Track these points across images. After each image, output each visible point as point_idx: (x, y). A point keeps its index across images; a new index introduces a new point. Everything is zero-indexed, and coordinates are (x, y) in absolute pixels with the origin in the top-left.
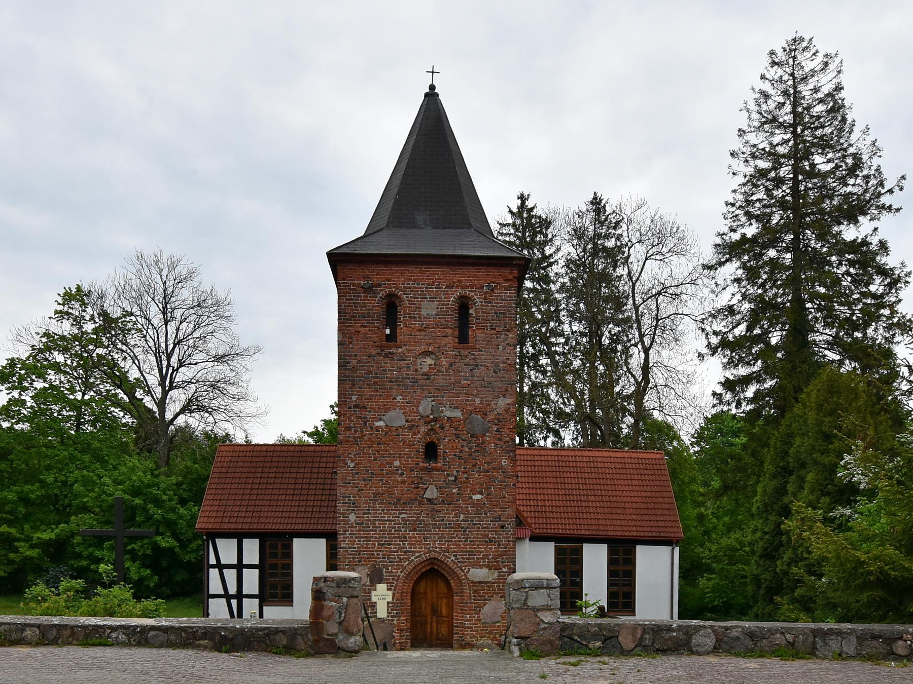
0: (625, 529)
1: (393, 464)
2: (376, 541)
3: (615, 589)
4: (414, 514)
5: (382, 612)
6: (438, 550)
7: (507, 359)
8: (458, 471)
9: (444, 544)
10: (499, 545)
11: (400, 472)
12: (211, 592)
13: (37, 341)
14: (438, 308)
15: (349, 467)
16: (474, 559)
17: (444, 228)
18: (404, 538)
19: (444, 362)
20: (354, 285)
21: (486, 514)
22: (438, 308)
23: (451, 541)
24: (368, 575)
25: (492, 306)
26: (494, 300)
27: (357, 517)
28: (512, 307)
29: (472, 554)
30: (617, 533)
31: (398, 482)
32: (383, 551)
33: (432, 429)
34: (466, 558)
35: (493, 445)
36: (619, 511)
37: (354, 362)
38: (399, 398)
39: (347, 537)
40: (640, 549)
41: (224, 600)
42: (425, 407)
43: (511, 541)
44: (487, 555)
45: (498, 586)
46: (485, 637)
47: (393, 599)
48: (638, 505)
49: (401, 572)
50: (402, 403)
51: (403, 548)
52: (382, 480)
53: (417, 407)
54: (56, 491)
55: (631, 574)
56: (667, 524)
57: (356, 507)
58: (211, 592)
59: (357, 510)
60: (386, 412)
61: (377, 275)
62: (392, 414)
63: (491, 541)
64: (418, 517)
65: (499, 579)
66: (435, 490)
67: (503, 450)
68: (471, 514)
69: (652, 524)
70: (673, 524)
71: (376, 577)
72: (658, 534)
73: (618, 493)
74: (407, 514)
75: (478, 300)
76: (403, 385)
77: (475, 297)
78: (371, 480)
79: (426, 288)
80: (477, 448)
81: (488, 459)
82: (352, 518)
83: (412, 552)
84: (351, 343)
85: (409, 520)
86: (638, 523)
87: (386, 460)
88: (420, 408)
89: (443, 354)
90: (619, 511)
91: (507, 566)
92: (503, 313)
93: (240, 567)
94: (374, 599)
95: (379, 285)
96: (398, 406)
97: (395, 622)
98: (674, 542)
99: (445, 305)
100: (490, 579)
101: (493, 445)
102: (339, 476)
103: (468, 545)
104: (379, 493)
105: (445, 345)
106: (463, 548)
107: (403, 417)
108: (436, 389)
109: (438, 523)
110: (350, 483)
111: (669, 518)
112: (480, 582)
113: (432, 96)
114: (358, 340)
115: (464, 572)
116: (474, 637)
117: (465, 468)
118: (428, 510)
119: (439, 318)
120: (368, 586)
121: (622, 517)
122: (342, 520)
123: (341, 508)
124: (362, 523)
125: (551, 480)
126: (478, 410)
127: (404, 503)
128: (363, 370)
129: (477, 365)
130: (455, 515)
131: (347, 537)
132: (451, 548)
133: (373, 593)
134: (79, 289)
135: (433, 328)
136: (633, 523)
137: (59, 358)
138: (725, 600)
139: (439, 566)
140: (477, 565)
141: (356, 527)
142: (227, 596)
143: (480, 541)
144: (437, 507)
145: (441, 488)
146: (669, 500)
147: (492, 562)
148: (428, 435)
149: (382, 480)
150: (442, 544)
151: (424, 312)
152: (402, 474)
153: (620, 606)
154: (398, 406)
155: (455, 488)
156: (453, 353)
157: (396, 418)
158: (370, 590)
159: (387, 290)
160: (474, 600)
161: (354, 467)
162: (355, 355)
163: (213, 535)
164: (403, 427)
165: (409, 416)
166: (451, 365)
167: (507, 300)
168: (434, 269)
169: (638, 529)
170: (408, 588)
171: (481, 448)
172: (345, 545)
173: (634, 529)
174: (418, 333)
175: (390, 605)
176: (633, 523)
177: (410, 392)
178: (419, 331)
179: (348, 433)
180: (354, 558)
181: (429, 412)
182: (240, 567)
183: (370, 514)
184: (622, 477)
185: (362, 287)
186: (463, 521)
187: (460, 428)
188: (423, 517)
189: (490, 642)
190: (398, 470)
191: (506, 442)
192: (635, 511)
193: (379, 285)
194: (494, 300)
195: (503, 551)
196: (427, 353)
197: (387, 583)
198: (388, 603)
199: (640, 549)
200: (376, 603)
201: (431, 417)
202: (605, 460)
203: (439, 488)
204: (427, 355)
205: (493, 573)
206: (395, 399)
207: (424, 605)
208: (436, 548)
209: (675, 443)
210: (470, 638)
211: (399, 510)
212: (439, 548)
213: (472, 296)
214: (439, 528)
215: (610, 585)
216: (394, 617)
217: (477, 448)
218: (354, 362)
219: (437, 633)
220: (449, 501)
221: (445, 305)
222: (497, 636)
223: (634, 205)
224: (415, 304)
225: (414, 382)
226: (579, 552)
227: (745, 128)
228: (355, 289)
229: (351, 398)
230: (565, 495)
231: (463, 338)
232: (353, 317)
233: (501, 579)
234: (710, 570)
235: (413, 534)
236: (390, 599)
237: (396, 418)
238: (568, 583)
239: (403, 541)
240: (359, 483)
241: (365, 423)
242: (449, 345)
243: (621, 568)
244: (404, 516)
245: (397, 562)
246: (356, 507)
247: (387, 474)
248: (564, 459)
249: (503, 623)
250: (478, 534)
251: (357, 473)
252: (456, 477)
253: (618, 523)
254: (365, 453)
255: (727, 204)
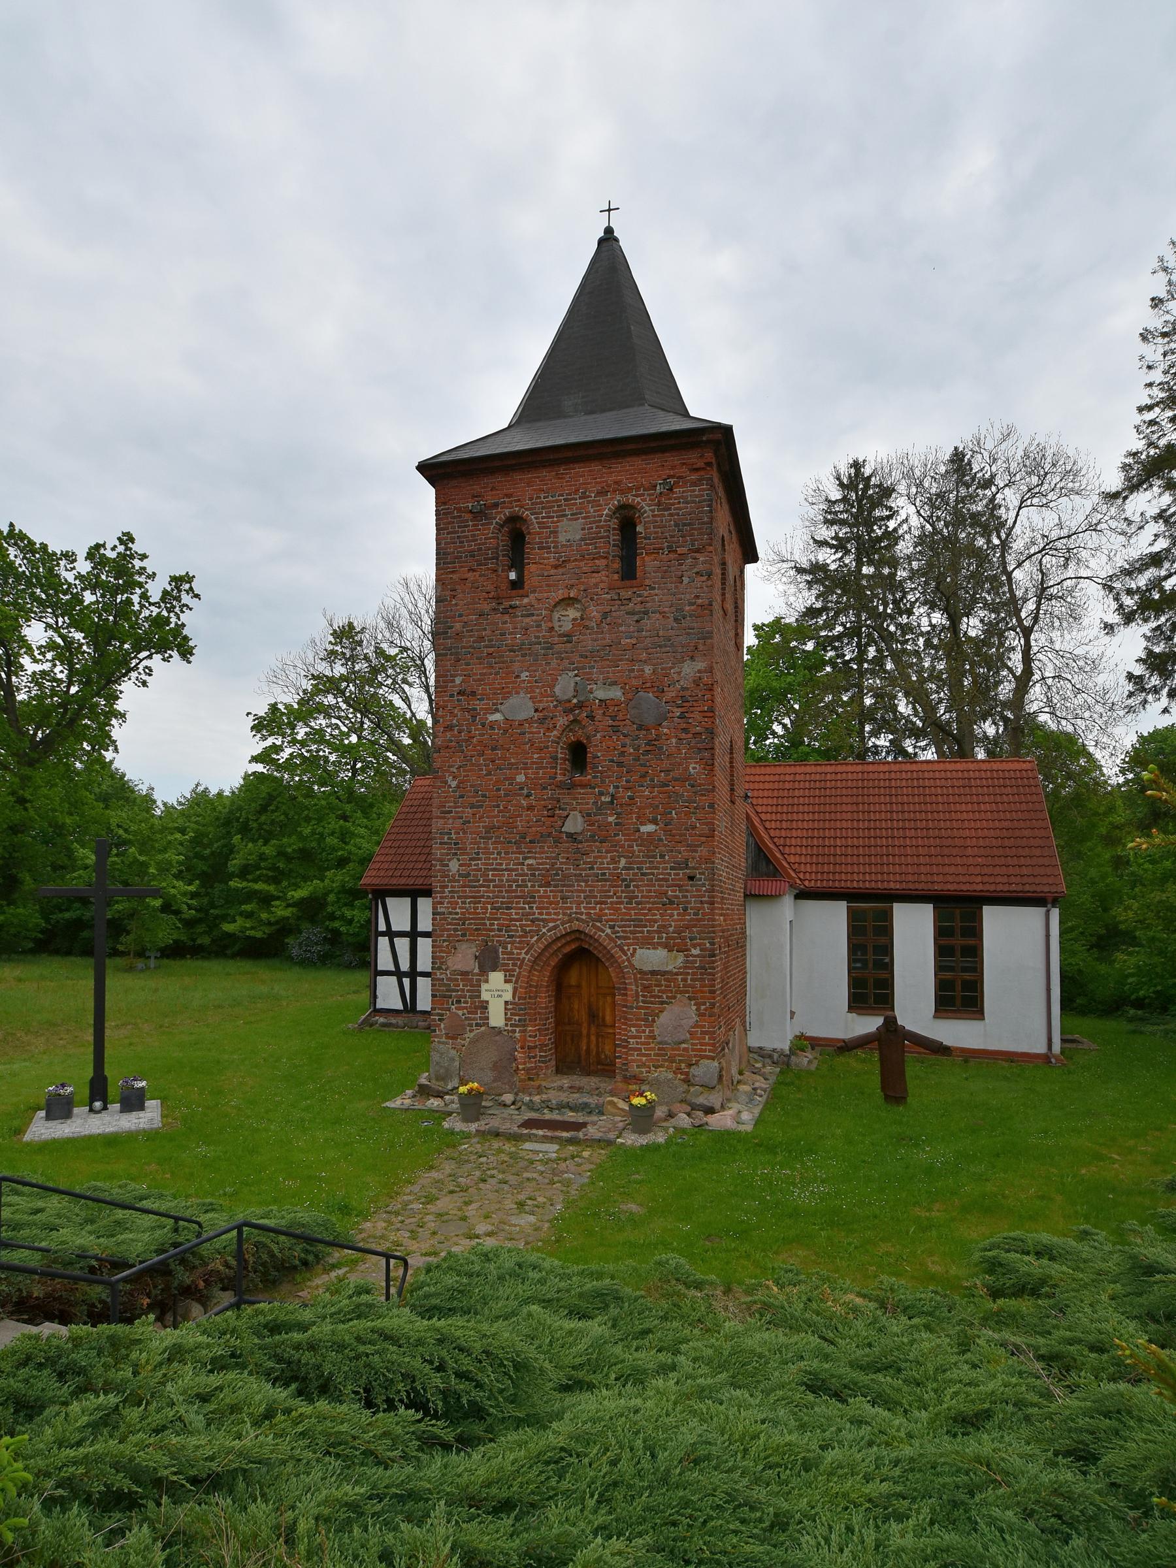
0: (961, 878)
1: (515, 779)
2: (488, 903)
3: (948, 975)
4: (547, 858)
5: (497, 1018)
6: (584, 917)
7: (697, 597)
8: (617, 787)
9: (594, 908)
10: (685, 909)
11: (525, 792)
12: (379, 968)
13: (308, 685)
14: (583, 529)
15: (450, 786)
16: (642, 932)
17: (603, 411)
18: (530, 898)
19: (594, 612)
20: (459, 510)
21: (662, 856)
22: (583, 529)
23: (605, 903)
24: (476, 957)
25: (671, 515)
26: (673, 504)
27: (461, 865)
28: (702, 512)
29: (639, 924)
30: (949, 887)
31: (523, 808)
32: (498, 919)
33: (575, 721)
34: (631, 932)
35: (674, 740)
36: (955, 851)
37: (458, 626)
38: (524, 675)
39: (445, 897)
40: (989, 913)
41: (395, 978)
42: (565, 686)
43: (707, 902)
44: (664, 926)
45: (685, 980)
46: (662, 1066)
47: (514, 997)
48: (987, 842)
49: (526, 953)
50: (529, 682)
51: (529, 914)
52: (498, 806)
53: (552, 687)
54: (314, 844)
55: (975, 952)
56: (1037, 871)
57: (459, 849)
58: (379, 968)
59: (462, 854)
60: (505, 698)
61: (491, 490)
62: (514, 700)
63: (672, 903)
64: (553, 864)
65: (685, 968)
66: (580, 819)
67: (692, 748)
68: (638, 857)
69: (1011, 871)
70: (1049, 871)
71: (488, 961)
72: (1020, 888)
73: (955, 824)
74: (535, 858)
75: (647, 508)
76: (530, 655)
77: (643, 504)
78: (481, 806)
79: (565, 500)
80: (648, 748)
81: (666, 764)
82: (454, 866)
83: (543, 920)
84: (454, 597)
85: (538, 869)
86: (986, 870)
87: (505, 774)
88: (557, 690)
89: (592, 599)
90: (955, 851)
91: (699, 945)
92: (690, 524)
93: (413, 935)
94: (485, 996)
95: (496, 505)
96: (523, 688)
97: (517, 1035)
98: (1050, 900)
99: (594, 522)
100: (670, 968)
101: (674, 740)
102: (436, 802)
103: (634, 909)
104: (494, 827)
105: (596, 585)
106: (625, 914)
107: (530, 704)
108: (581, 656)
109: (584, 873)
110: (451, 812)
111: (1041, 861)
112: (653, 973)
113: (608, 239)
114: (463, 592)
115: (626, 955)
116: (644, 1065)
117: (627, 781)
118: (568, 852)
119: (586, 544)
120: (478, 975)
121: (958, 860)
122: (439, 871)
123: (438, 852)
124: (469, 875)
125: (849, 808)
126: (648, 685)
127: (531, 842)
128: (471, 636)
129: (646, 613)
130: (612, 859)
131: (445, 897)
132: (606, 915)
133: (484, 987)
134: (351, 625)
135: (576, 560)
136: (977, 870)
137: (330, 700)
138: (1159, 988)
139: (590, 945)
140: (647, 943)
141: (458, 881)
142: (398, 973)
143: (653, 903)
144: (584, 846)
145: (589, 815)
146: (1043, 833)
147: (674, 938)
148: (571, 730)
149: (498, 806)
150: (590, 908)
151: (562, 538)
152: (528, 796)
153: (958, 1002)
154: (523, 688)
155: (612, 815)
156: (608, 596)
157: (520, 707)
158: (479, 981)
159: (507, 512)
160: (644, 1002)
161: (458, 787)
162: (461, 616)
163: (382, 894)
164: (530, 721)
165: (540, 701)
166: (605, 615)
167: (694, 502)
168: (579, 469)
169: (986, 879)
170: (544, 977)
171: (654, 746)
172: (443, 910)
173: (979, 879)
174: (553, 572)
175: (510, 1007)
176: (977, 870)
177: (541, 665)
178: (556, 567)
179: (448, 735)
180: (456, 930)
181: (571, 693)
182: (413, 935)
183: (480, 859)
184: (963, 799)
185: (471, 512)
186: (625, 868)
187: (620, 717)
188: (562, 863)
189: (671, 1076)
190: (522, 789)
191: (696, 735)
192: (982, 851)
193: (496, 505)
194: (673, 504)
195: (692, 920)
196: (568, 601)
197: (505, 971)
198: (506, 1003)
199: (989, 913)
200: (487, 1002)
201: (575, 701)
202: (937, 775)
203: (587, 815)
204: (568, 605)
205: (676, 957)
206: (518, 676)
207: (576, 1007)
208: (582, 914)
209: (1082, 762)
210: (638, 1066)
211: (523, 853)
212: (587, 914)
213: (639, 503)
214: (586, 881)
215: (939, 968)
216: (516, 1026)
217: (648, 748)
218: (458, 626)
219: (598, 1053)
220: (601, 835)
221: (594, 522)
222: (683, 1065)
223: (998, 436)
224: (549, 527)
225: (548, 648)
226: (888, 917)
227: (1163, 294)
228: (460, 517)
229: (453, 681)
230: (869, 829)
231: (629, 572)
232: (456, 558)
233: (689, 968)
234: (1134, 941)
235: (546, 891)
236: (508, 996)
237: (520, 707)
238: (871, 965)
239: (529, 903)
240: (463, 812)
241: (474, 717)
242: (602, 585)
243: (958, 941)
244: (530, 862)
245: (520, 937)
246: (459, 849)
247: (506, 795)
248: (871, 776)
249: (693, 1044)
250: (650, 891)
251: (462, 797)
252: (612, 796)
253: (952, 869)
254: (473, 765)
255: (1140, 410)
